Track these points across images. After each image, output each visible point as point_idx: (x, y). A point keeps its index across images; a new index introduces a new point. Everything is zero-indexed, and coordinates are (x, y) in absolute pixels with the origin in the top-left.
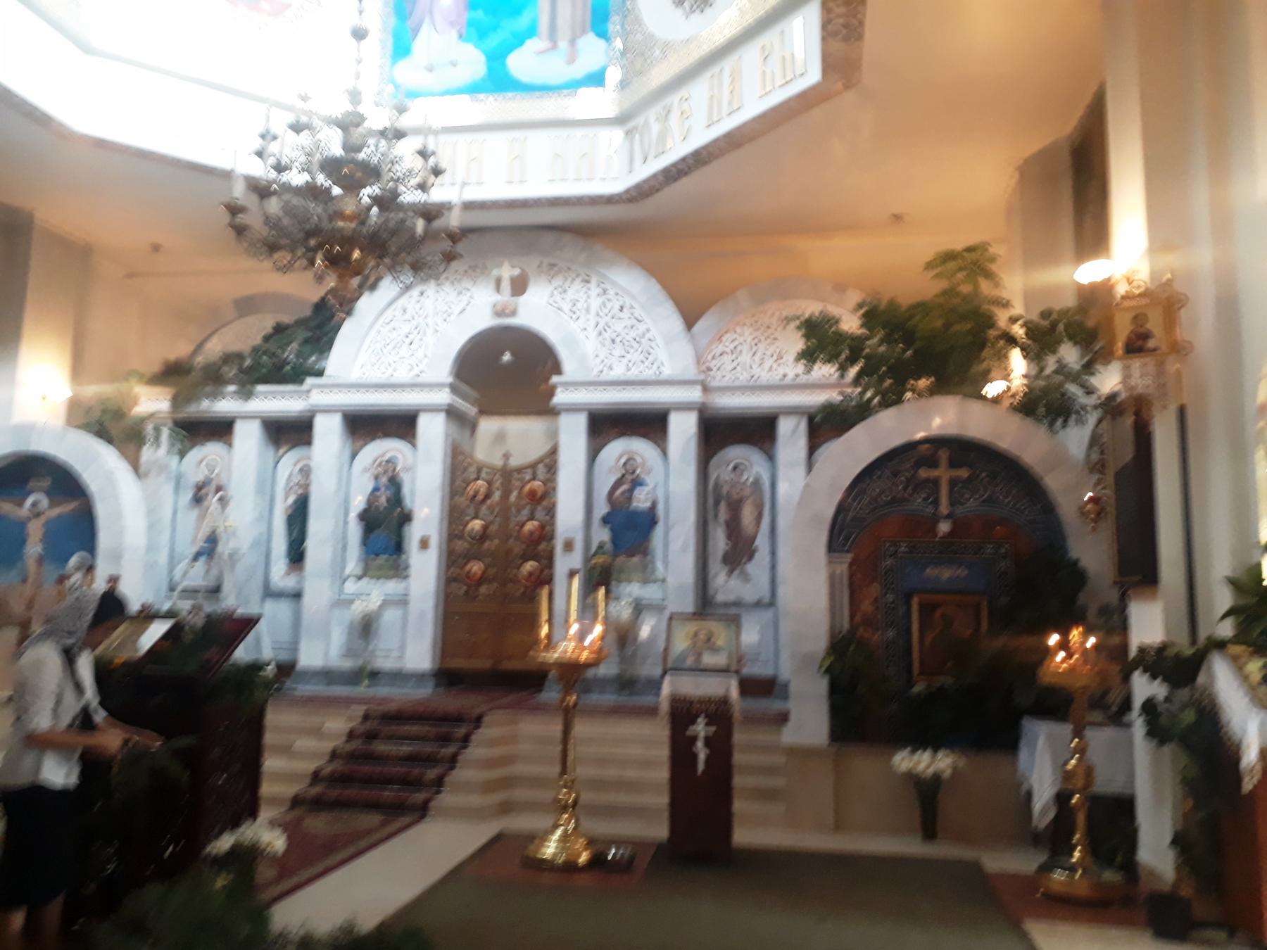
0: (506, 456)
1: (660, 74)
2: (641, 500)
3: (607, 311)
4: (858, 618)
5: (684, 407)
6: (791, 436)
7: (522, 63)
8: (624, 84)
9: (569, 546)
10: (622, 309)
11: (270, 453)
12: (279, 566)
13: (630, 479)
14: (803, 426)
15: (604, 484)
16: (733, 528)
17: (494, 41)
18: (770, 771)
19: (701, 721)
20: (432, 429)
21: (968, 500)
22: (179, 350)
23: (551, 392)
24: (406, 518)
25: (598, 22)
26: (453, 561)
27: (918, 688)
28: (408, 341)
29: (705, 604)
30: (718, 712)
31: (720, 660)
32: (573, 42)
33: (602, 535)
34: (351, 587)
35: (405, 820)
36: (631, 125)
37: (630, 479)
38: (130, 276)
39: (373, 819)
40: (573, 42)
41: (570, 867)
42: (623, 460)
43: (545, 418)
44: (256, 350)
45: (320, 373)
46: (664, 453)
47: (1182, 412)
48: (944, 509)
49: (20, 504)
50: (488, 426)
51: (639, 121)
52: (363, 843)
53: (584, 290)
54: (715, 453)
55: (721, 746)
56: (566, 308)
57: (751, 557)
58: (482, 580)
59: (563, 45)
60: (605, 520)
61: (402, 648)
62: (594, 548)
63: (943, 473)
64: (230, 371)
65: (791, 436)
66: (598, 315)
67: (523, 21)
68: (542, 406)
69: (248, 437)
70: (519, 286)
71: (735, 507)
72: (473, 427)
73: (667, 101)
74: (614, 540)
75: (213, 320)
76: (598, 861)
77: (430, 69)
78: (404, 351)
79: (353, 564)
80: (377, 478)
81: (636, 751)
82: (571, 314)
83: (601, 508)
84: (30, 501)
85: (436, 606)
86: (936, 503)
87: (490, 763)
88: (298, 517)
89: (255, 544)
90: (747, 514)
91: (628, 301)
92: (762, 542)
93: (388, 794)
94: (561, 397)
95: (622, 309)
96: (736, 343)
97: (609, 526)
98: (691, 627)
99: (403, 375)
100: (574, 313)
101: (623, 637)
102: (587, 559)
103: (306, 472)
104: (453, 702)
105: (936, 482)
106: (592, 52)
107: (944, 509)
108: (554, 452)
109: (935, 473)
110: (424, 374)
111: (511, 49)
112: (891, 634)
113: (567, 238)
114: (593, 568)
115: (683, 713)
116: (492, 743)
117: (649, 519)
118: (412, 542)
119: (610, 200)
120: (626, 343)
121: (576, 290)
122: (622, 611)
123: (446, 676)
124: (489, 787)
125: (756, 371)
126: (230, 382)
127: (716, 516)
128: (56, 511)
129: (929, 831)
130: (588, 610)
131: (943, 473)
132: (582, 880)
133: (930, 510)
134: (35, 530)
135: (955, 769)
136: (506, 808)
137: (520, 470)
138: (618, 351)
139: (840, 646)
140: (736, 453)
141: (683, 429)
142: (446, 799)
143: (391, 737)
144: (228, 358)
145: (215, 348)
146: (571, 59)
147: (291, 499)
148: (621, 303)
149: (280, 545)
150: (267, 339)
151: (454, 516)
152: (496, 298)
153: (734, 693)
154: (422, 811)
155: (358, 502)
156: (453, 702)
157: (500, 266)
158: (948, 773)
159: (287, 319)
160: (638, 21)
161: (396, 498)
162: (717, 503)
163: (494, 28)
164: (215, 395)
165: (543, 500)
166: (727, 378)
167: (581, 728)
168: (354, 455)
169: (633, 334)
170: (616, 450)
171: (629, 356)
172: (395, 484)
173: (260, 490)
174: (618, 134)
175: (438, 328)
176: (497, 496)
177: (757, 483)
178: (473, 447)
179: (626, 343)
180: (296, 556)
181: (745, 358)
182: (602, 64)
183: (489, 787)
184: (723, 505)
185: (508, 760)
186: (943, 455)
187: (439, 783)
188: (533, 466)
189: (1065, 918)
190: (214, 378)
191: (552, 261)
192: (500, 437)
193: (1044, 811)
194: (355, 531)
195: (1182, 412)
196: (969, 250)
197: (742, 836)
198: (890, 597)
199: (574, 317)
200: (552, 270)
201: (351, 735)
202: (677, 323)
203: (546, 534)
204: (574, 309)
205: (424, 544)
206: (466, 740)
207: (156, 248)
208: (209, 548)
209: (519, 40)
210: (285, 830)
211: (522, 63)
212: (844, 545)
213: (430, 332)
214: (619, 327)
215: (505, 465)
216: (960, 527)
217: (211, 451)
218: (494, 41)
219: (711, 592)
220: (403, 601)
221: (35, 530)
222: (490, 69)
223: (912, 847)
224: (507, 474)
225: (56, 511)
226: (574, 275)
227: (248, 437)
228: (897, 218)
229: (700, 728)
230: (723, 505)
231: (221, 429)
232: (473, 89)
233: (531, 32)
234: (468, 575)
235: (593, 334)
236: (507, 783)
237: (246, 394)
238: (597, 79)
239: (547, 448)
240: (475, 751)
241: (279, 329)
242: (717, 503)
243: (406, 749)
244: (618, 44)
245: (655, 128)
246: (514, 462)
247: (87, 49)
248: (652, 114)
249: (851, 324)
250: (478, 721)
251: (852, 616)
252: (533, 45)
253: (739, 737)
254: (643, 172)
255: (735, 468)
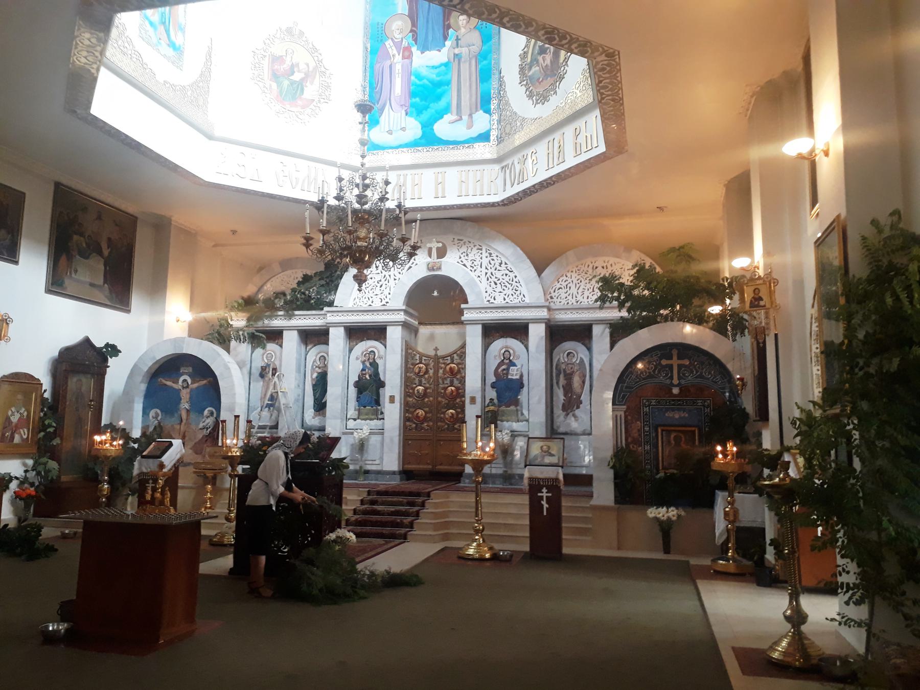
0: (436, 349)
1: (519, 139)
2: (514, 374)
3: (492, 266)
4: (630, 440)
5: (537, 321)
6: (600, 335)
7: (442, 129)
8: (500, 140)
9: (473, 400)
10: (501, 264)
11: (303, 347)
12: (310, 412)
13: (508, 361)
14: (608, 331)
15: (492, 365)
16: (568, 389)
17: (425, 116)
18: (585, 520)
19: (544, 490)
20: (395, 335)
21: (687, 377)
22: (250, 290)
23: (461, 312)
24: (382, 384)
25: (484, 104)
26: (407, 408)
27: (661, 474)
28: (379, 285)
29: (553, 433)
30: (552, 485)
31: (554, 460)
32: (470, 115)
33: (492, 394)
34: (351, 424)
35: (398, 541)
36: (504, 164)
37: (508, 361)
38: (215, 246)
39: (380, 541)
40: (470, 115)
41: (482, 560)
42: (503, 351)
43: (456, 326)
44: (294, 290)
45: (331, 304)
46: (527, 347)
47: (776, 335)
48: (676, 381)
49: (176, 382)
50: (424, 331)
51: (509, 161)
52: (379, 550)
53: (479, 254)
54: (556, 347)
55: (555, 504)
56: (468, 264)
57: (578, 407)
58: (425, 419)
59: (465, 117)
60: (493, 386)
61: (381, 458)
62: (487, 401)
63: (675, 362)
64: (280, 303)
65: (600, 335)
66: (486, 268)
67: (442, 103)
68: (455, 318)
69: (291, 339)
70: (442, 253)
71: (569, 377)
72: (416, 332)
73: (524, 153)
74: (499, 397)
75: (262, 268)
76: (495, 557)
77: (390, 132)
78: (378, 291)
79: (352, 413)
80: (363, 362)
81: (513, 510)
82: (471, 268)
83: (491, 378)
84: (181, 379)
85: (400, 435)
86: (671, 378)
87: (436, 515)
88: (321, 384)
89: (297, 400)
90: (576, 380)
91: (504, 260)
92: (584, 397)
93: (387, 530)
94: (467, 316)
95: (501, 264)
96: (567, 283)
97: (495, 389)
98: (540, 444)
99: (377, 305)
100: (473, 267)
101: (505, 451)
102: (484, 407)
103: (323, 358)
104: (413, 486)
105: (671, 367)
106: (482, 122)
107: (676, 381)
108: (463, 346)
109: (675, 357)
110: (388, 304)
111: (436, 121)
112: (647, 448)
113: (469, 223)
114: (85, 209)
115: (535, 486)
116: (436, 505)
117: (519, 384)
118: (384, 400)
119: (493, 205)
120: (503, 285)
121: (474, 254)
122: (505, 437)
123: (406, 474)
124: (436, 527)
125: (580, 298)
126: (279, 309)
127: (558, 383)
128: (196, 385)
129: (667, 551)
130: (486, 436)
131: (675, 362)
132: (488, 564)
133: (668, 382)
134: (185, 395)
135: (679, 516)
136: (446, 537)
137: (443, 357)
138: (499, 288)
139: (619, 453)
140: (569, 346)
141: (537, 333)
142: (416, 532)
143: (383, 503)
144: (280, 294)
145: (270, 288)
146: (470, 126)
147: (315, 375)
148: (500, 262)
149: (310, 400)
150: (299, 283)
151: (408, 384)
152: (429, 260)
153: (561, 477)
154: (404, 537)
155: (354, 378)
156: (413, 486)
157: (430, 242)
158: (674, 518)
159: (309, 273)
160: (507, 103)
161: (376, 375)
162: (558, 375)
163: (426, 108)
164: (270, 317)
165: (458, 374)
166: (562, 303)
167: (485, 499)
168: (351, 350)
169: (507, 278)
170: (499, 345)
171: (505, 292)
172: (374, 365)
173: (298, 371)
174: (497, 167)
175: (396, 278)
176: (431, 372)
177: (582, 361)
178: (416, 343)
179: (503, 285)
180: (320, 406)
181: (574, 290)
182: (488, 128)
183: (436, 527)
184: (562, 376)
185: (444, 514)
186: (675, 353)
187: (411, 526)
188: (451, 355)
189: (722, 579)
190: (270, 306)
191: (460, 238)
192: (432, 337)
193: (721, 535)
194: (353, 391)
195: (776, 335)
196: (682, 247)
197: (566, 550)
198: (647, 429)
199: (473, 270)
200: (460, 242)
201: (362, 502)
202: (533, 272)
203: (460, 393)
204: (473, 265)
205: (392, 400)
206: (423, 505)
207: (234, 232)
208: (272, 402)
209: (440, 116)
210: (610, 327)
211: (442, 129)
212: (622, 401)
213: (392, 280)
214: (498, 274)
215: (436, 355)
216: (684, 390)
217: (271, 347)
218: (425, 116)
219: (555, 427)
220: (381, 431)
221: (185, 395)
222: (424, 133)
223: (660, 556)
224: (437, 358)
225: (196, 385)
226: (472, 246)
227: (291, 339)
228: (660, 208)
229: (544, 493)
230: (562, 376)
231: (276, 336)
232: (414, 145)
233: (447, 110)
234: (417, 417)
235: (484, 278)
236: (447, 525)
237: (290, 316)
238: (484, 137)
239: (459, 344)
240: (429, 509)
241: (306, 279)
242: (558, 375)
243: (392, 509)
244: (495, 117)
245: (518, 167)
246: (440, 353)
247: (210, 137)
248: (516, 159)
249: (627, 279)
250: (428, 495)
251: (626, 439)
252: (448, 117)
253: (565, 503)
254: (511, 191)
255: (569, 354)
